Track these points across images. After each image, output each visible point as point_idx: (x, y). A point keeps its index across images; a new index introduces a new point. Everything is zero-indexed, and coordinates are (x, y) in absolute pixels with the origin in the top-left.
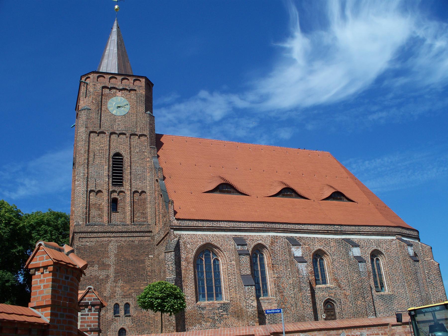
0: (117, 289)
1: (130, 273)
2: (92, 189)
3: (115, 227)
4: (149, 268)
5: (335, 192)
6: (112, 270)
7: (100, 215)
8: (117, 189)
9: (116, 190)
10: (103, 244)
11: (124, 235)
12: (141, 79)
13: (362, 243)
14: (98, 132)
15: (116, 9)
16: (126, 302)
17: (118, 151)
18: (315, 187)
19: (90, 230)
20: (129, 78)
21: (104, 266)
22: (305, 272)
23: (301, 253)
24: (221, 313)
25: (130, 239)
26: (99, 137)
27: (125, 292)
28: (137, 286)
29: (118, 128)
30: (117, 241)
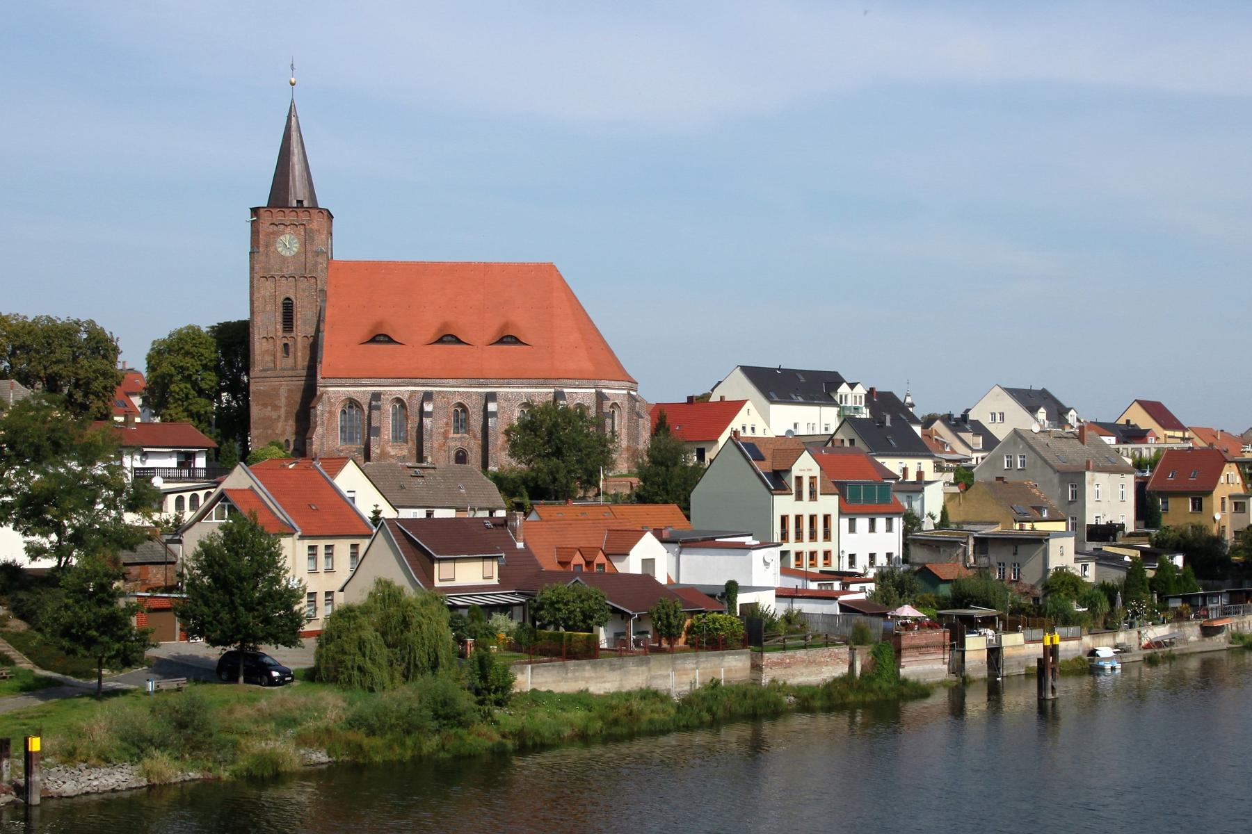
6: (283, 411)
21: (276, 408)
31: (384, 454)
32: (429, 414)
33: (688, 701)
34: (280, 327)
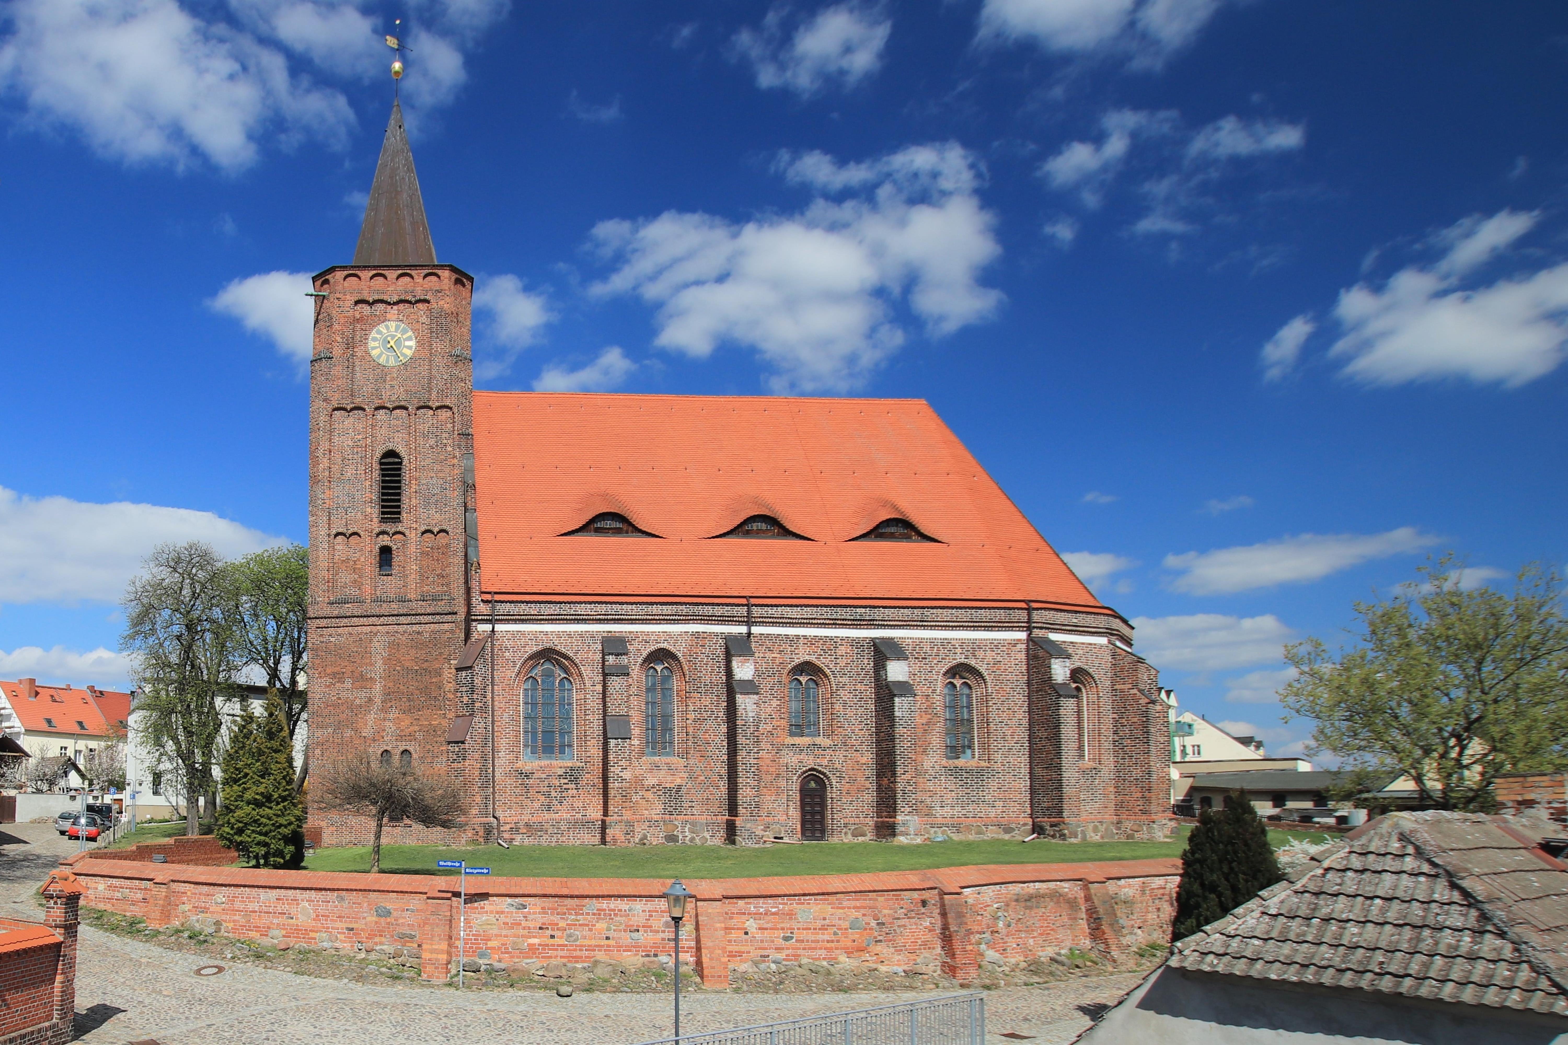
0: (387, 723)
1: (412, 694)
2: (340, 530)
3: (384, 605)
4: (451, 685)
6: (378, 688)
7: (355, 581)
8: (390, 528)
9: (388, 529)
10: (361, 640)
11: (403, 619)
12: (439, 272)
14: (349, 408)
15: (397, 73)
16: (404, 748)
17: (391, 446)
18: (829, 509)
19: (335, 613)
20: (413, 273)
21: (362, 680)
22: (751, 714)
23: (752, 673)
24: (565, 786)
25: (414, 629)
26: (351, 420)
27: (402, 731)
28: (426, 719)
30: (388, 633)
31: (615, 840)
32: (750, 687)
33: (565, 704)
34: (374, 512)
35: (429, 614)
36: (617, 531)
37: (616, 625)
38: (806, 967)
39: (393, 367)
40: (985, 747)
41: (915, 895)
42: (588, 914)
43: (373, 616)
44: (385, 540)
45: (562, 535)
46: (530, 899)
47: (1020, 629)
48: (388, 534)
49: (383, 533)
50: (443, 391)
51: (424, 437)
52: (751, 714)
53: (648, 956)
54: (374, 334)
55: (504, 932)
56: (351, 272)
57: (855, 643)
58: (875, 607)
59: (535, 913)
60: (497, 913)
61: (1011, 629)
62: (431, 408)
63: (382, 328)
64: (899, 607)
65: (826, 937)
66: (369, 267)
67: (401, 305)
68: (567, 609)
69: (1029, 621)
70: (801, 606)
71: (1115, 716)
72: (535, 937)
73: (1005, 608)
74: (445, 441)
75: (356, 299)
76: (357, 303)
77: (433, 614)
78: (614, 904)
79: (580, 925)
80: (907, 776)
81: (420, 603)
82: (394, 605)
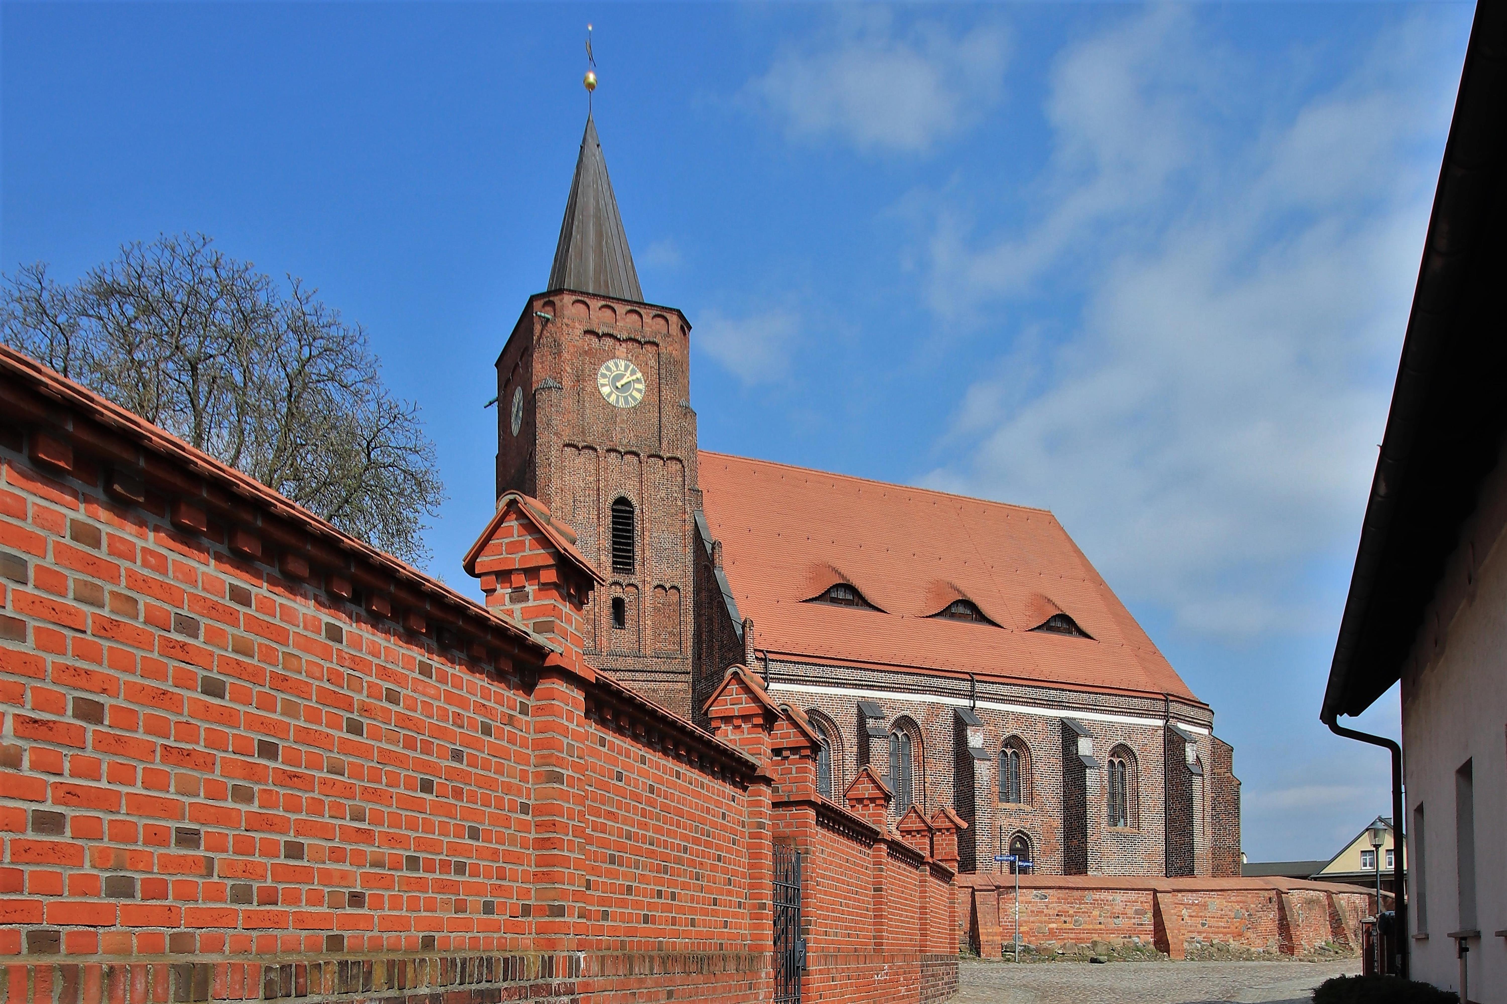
3: (620, 659)
5: (1058, 615)
13: (1098, 730)
22: (985, 779)
23: (982, 741)
29: (623, 438)
35: (664, 672)
36: (848, 603)
37: (868, 691)
38: (1216, 946)
39: (623, 409)
40: (1137, 816)
41: (1266, 894)
42: (1087, 903)
43: (610, 670)
44: (617, 592)
45: (803, 601)
46: (1050, 891)
47: (1160, 717)
48: (621, 585)
49: (615, 583)
50: (673, 441)
51: (655, 488)
52: (985, 779)
53: (1125, 937)
54: (603, 370)
55: (1032, 919)
56: (580, 298)
57: (1048, 720)
58: (1063, 690)
59: (1052, 903)
60: (1026, 903)
61: (1154, 717)
62: (662, 458)
63: (611, 364)
64: (1080, 692)
65: (1222, 924)
66: (599, 296)
67: (630, 344)
68: (828, 672)
69: (1167, 711)
70: (1010, 684)
71: (1213, 795)
72: (1053, 922)
73: (1151, 699)
74: (676, 495)
75: (586, 328)
76: (587, 332)
77: (668, 672)
78: (1104, 895)
79: (1083, 912)
80: (1094, 838)
81: (655, 660)
82: (629, 660)
